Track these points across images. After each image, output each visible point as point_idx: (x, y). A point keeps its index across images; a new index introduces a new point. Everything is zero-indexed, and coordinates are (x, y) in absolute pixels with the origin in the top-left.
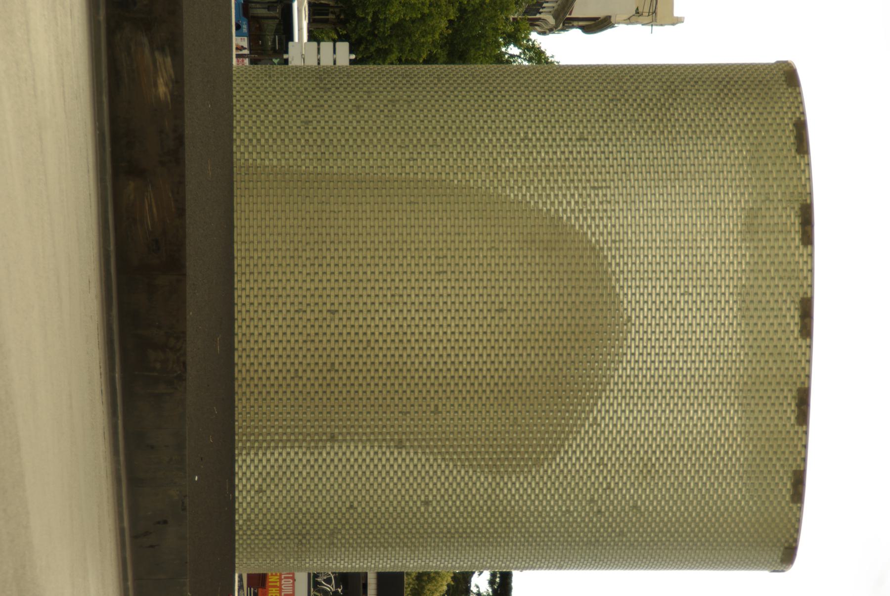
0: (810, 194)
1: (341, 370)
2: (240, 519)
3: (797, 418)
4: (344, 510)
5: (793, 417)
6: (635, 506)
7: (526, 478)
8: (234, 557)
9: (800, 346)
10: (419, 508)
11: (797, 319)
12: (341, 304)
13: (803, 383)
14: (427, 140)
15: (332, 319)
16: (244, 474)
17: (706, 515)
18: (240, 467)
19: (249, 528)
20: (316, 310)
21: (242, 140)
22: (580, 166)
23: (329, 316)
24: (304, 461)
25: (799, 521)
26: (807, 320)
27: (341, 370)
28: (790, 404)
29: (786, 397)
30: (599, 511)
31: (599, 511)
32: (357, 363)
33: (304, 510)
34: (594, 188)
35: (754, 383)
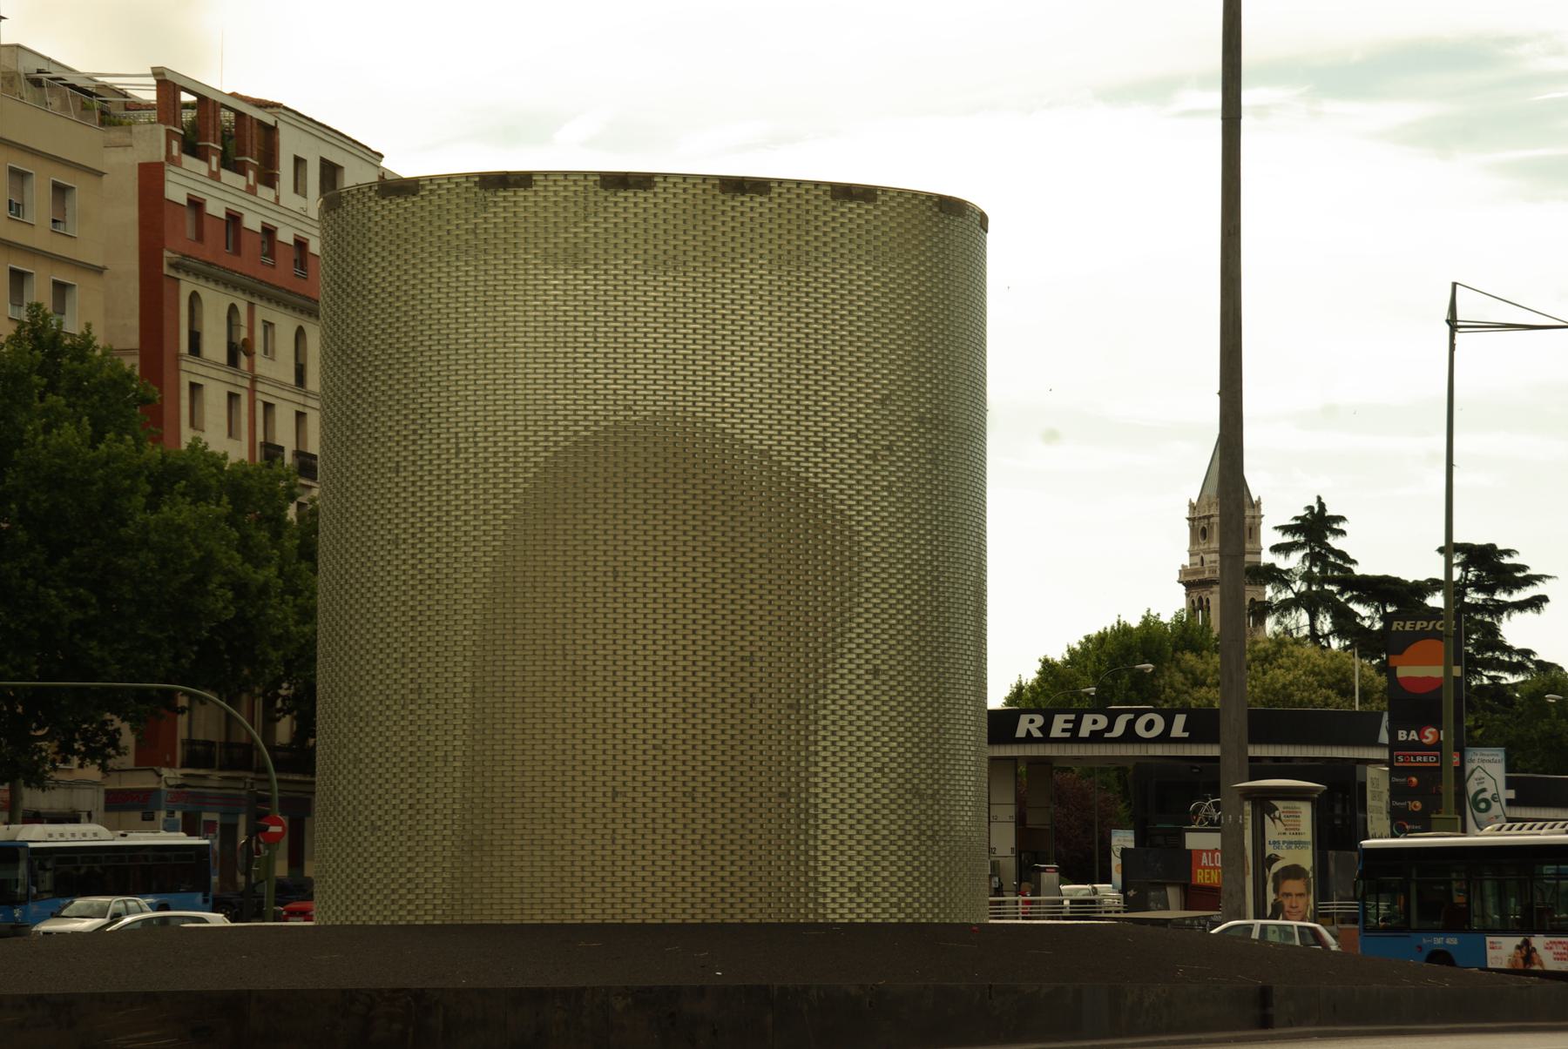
0: (468, 176)
1: (692, 784)
2: (896, 917)
3: (868, 201)
4: (885, 780)
5: (759, 199)
6: (882, 402)
7: (867, 549)
8: (952, 925)
9: (780, 195)
10: (884, 683)
11: (630, 194)
12: (604, 784)
13: (714, 186)
14: (396, 671)
15: (624, 794)
16: (868, 910)
17: (908, 312)
18: (842, 916)
19: (909, 905)
20: (672, 816)
21: (409, 912)
22: (448, 471)
23: (620, 799)
24: (853, 832)
25: (901, 192)
26: (631, 181)
27: (692, 784)
28: (742, 203)
29: (733, 208)
30: (888, 448)
31: (888, 448)
32: (704, 763)
33: (900, 832)
34: (457, 454)
35: (714, 248)
